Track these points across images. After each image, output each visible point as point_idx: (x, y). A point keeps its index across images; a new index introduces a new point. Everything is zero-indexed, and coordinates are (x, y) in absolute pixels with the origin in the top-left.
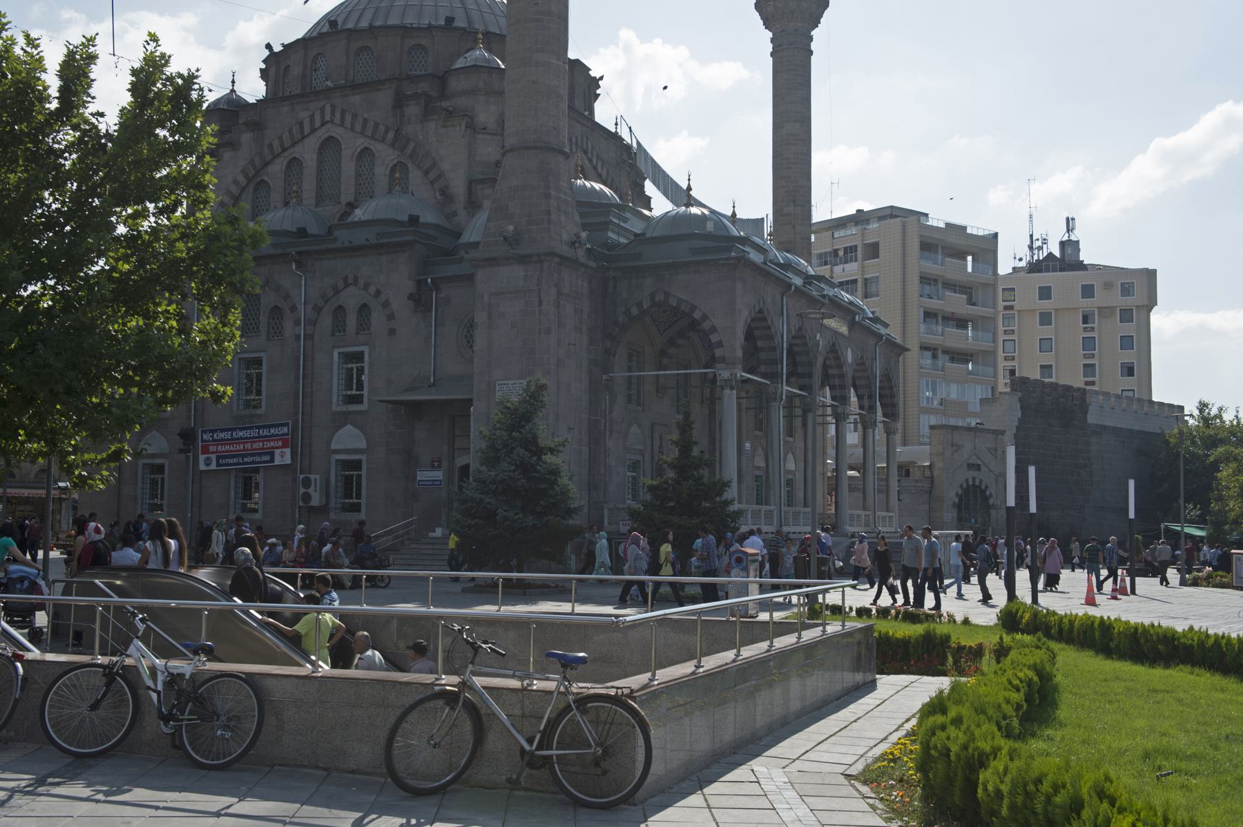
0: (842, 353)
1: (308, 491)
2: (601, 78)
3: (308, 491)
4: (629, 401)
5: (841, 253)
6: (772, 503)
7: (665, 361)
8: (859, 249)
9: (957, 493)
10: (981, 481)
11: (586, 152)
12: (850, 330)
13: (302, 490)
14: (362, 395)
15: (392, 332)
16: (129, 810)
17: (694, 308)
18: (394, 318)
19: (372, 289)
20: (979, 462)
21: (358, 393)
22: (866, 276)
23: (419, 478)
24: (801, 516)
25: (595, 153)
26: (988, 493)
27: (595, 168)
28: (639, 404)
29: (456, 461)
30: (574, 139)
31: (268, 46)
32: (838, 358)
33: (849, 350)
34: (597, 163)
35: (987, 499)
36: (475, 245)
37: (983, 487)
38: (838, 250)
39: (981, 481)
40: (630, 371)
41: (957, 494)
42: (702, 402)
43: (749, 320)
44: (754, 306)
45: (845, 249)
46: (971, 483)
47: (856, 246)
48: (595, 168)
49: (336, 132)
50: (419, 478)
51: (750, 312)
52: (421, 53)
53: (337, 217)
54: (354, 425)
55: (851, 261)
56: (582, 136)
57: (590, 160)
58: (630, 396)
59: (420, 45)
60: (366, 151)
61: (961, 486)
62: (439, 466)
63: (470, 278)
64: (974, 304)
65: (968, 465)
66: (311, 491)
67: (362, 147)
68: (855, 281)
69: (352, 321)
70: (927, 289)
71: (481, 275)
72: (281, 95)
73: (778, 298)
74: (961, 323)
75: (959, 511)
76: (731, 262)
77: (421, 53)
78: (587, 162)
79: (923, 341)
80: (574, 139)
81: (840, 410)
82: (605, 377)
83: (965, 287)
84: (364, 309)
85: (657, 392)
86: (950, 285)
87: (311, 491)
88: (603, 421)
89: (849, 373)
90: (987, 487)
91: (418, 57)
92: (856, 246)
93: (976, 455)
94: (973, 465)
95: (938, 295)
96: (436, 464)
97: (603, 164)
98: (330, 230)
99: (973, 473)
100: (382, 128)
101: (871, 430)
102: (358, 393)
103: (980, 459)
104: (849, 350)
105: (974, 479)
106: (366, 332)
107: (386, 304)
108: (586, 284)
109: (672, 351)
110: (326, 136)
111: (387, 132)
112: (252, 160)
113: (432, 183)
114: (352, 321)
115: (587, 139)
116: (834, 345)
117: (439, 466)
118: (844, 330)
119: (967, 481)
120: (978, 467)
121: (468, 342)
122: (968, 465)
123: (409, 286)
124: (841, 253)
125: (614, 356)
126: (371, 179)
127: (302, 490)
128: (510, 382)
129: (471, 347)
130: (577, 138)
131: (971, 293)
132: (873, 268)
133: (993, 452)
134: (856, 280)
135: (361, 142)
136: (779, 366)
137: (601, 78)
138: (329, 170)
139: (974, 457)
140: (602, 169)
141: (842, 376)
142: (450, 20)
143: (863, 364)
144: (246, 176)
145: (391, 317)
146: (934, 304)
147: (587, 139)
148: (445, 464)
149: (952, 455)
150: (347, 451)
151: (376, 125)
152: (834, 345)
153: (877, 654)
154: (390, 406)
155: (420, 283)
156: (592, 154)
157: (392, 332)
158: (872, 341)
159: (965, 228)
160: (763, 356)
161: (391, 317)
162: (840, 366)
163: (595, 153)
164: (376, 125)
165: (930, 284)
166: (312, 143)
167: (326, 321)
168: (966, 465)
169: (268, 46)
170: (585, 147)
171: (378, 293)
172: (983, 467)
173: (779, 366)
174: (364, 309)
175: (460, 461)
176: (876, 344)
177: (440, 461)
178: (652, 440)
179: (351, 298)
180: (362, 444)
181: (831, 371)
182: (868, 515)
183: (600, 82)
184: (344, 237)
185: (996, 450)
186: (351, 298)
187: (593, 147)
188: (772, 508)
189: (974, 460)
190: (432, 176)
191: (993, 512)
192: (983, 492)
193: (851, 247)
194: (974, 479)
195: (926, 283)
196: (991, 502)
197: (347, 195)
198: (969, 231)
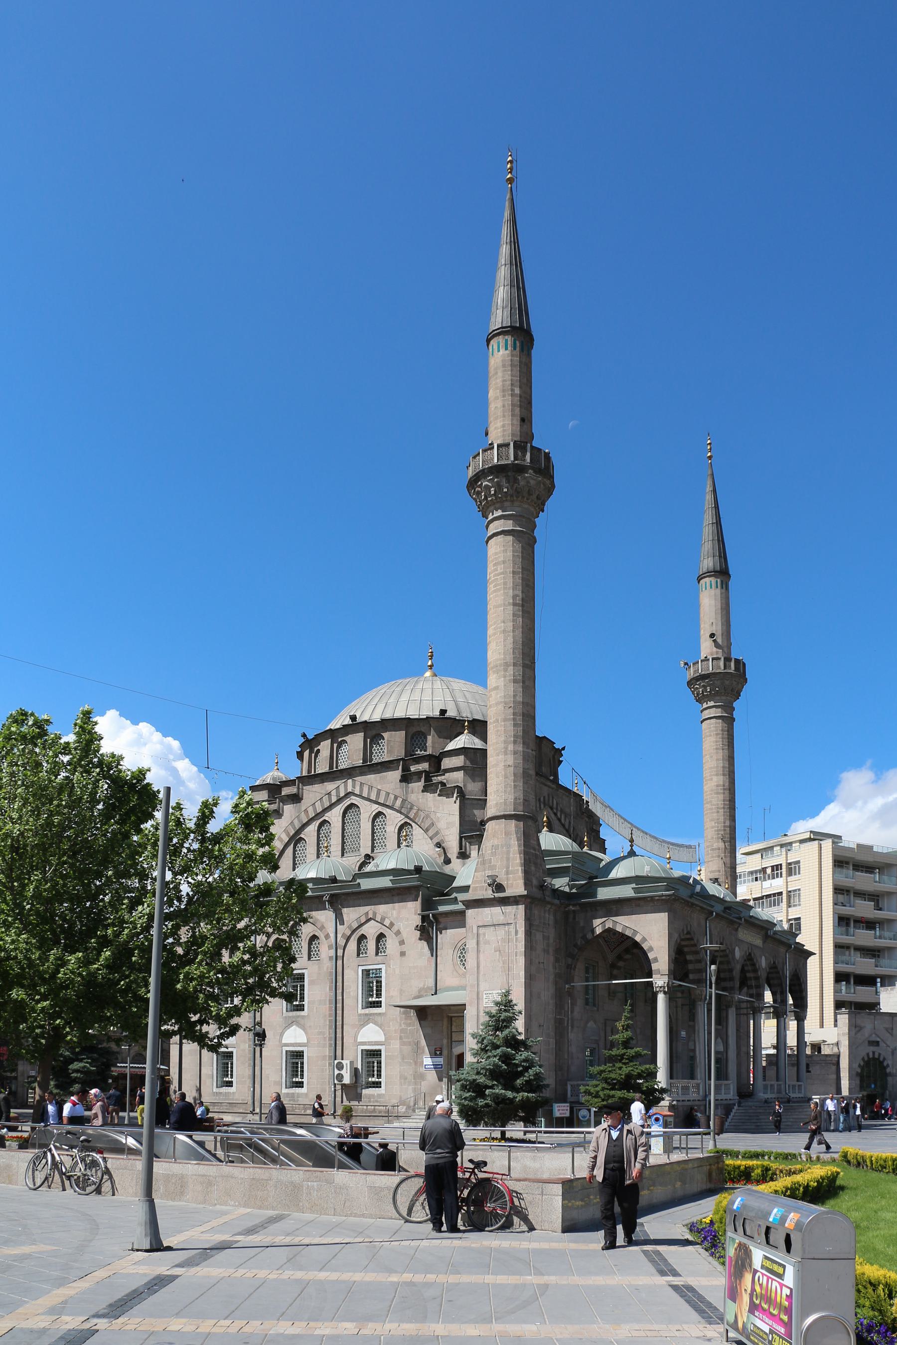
0: (757, 960)
1: (339, 1072)
2: (563, 749)
3: (339, 1072)
4: (587, 1003)
5: (769, 871)
6: (699, 1078)
7: (615, 972)
8: (784, 867)
9: (860, 1064)
10: (880, 1054)
11: (552, 808)
12: (764, 942)
13: (337, 1072)
14: (381, 1002)
15: (403, 954)
16: (479, 1132)
17: (635, 932)
18: (404, 943)
19: (387, 922)
20: (878, 1039)
21: (377, 999)
22: (789, 890)
23: (425, 1063)
24: (723, 1087)
25: (559, 809)
26: (885, 1064)
27: (559, 820)
28: (594, 1005)
29: (453, 1050)
30: (542, 799)
31: (304, 735)
32: (754, 965)
33: (763, 958)
34: (561, 816)
35: (885, 1068)
36: (466, 889)
37: (881, 1059)
38: (766, 868)
39: (880, 1054)
40: (587, 980)
41: (860, 1066)
42: (646, 1001)
43: (679, 941)
44: (683, 930)
45: (772, 867)
46: (871, 1056)
47: (781, 865)
48: (559, 820)
49: (354, 800)
50: (425, 1063)
51: (680, 935)
52: (421, 738)
53: (357, 868)
54: (376, 1023)
55: (777, 877)
56: (549, 795)
57: (555, 814)
58: (587, 1000)
59: (421, 732)
60: (379, 814)
61: (863, 1059)
62: (441, 1054)
63: (462, 913)
64: (880, 909)
65: (869, 1042)
66: (343, 1072)
67: (377, 811)
68: (780, 894)
69: (371, 945)
70: (841, 898)
71: (470, 913)
72: (313, 773)
73: (703, 922)
74: (870, 924)
75: (862, 1081)
76: (664, 898)
77: (421, 738)
78: (553, 816)
79: (838, 941)
80: (542, 799)
81: (756, 1005)
82: (567, 986)
83: (873, 895)
84: (381, 937)
85: (609, 995)
86: (860, 894)
87: (343, 1072)
88: (566, 1019)
89: (763, 974)
90: (884, 1059)
91: (419, 741)
92: (781, 865)
93: (876, 1034)
94: (873, 1042)
95: (850, 903)
96: (438, 1053)
97: (566, 817)
98: (354, 879)
99: (872, 1048)
100: (392, 797)
101: (782, 1019)
102: (377, 999)
103: (879, 1037)
104: (763, 958)
105: (874, 1053)
106: (383, 954)
107: (398, 933)
108: (552, 917)
109: (621, 964)
110: (349, 803)
111: (396, 798)
112: (292, 822)
113: (431, 838)
114: (371, 945)
115: (553, 798)
116: (750, 954)
117: (441, 1054)
118: (758, 942)
119: (868, 1054)
120: (877, 1044)
121: (461, 961)
122: (869, 1042)
123: (418, 921)
124: (769, 871)
125: (574, 970)
126: (384, 835)
127: (337, 1072)
128: (494, 992)
129: (464, 965)
130: (544, 797)
131: (878, 900)
132: (794, 883)
133: (890, 1031)
134: (782, 892)
135: (376, 808)
136: (704, 974)
137: (563, 749)
138: (351, 835)
139: (874, 1035)
140: (565, 820)
141: (757, 978)
142: (443, 712)
143: (776, 967)
144: (288, 834)
145: (402, 943)
146: (847, 911)
147: (553, 798)
148: (445, 1052)
149: (856, 1034)
150: (370, 1043)
151: (388, 794)
152: (750, 954)
153: (678, 1162)
154: (402, 1010)
155: (424, 918)
156: (557, 809)
157: (403, 954)
158: (782, 950)
159: (872, 847)
160: (691, 967)
161: (402, 943)
162: (755, 971)
163: (559, 809)
164: (388, 794)
165: (843, 894)
166: (338, 810)
167: (352, 945)
168: (867, 1042)
169: (304, 735)
170: (551, 804)
171: (392, 924)
172: (881, 1044)
173: (704, 974)
174: (381, 937)
175: (456, 1051)
176: (786, 951)
177: (441, 1050)
178: (605, 1032)
179: (371, 930)
180: (382, 1038)
181: (748, 975)
182: (780, 1085)
183: (563, 752)
184: (366, 884)
185: (892, 1029)
186: (371, 930)
187: (557, 804)
188: (699, 1081)
189: (874, 1038)
190: (431, 833)
191: (890, 1079)
192: (882, 1063)
193: (777, 866)
194: (874, 1053)
195: (839, 893)
196: (888, 1070)
197: (366, 849)
198: (875, 849)
